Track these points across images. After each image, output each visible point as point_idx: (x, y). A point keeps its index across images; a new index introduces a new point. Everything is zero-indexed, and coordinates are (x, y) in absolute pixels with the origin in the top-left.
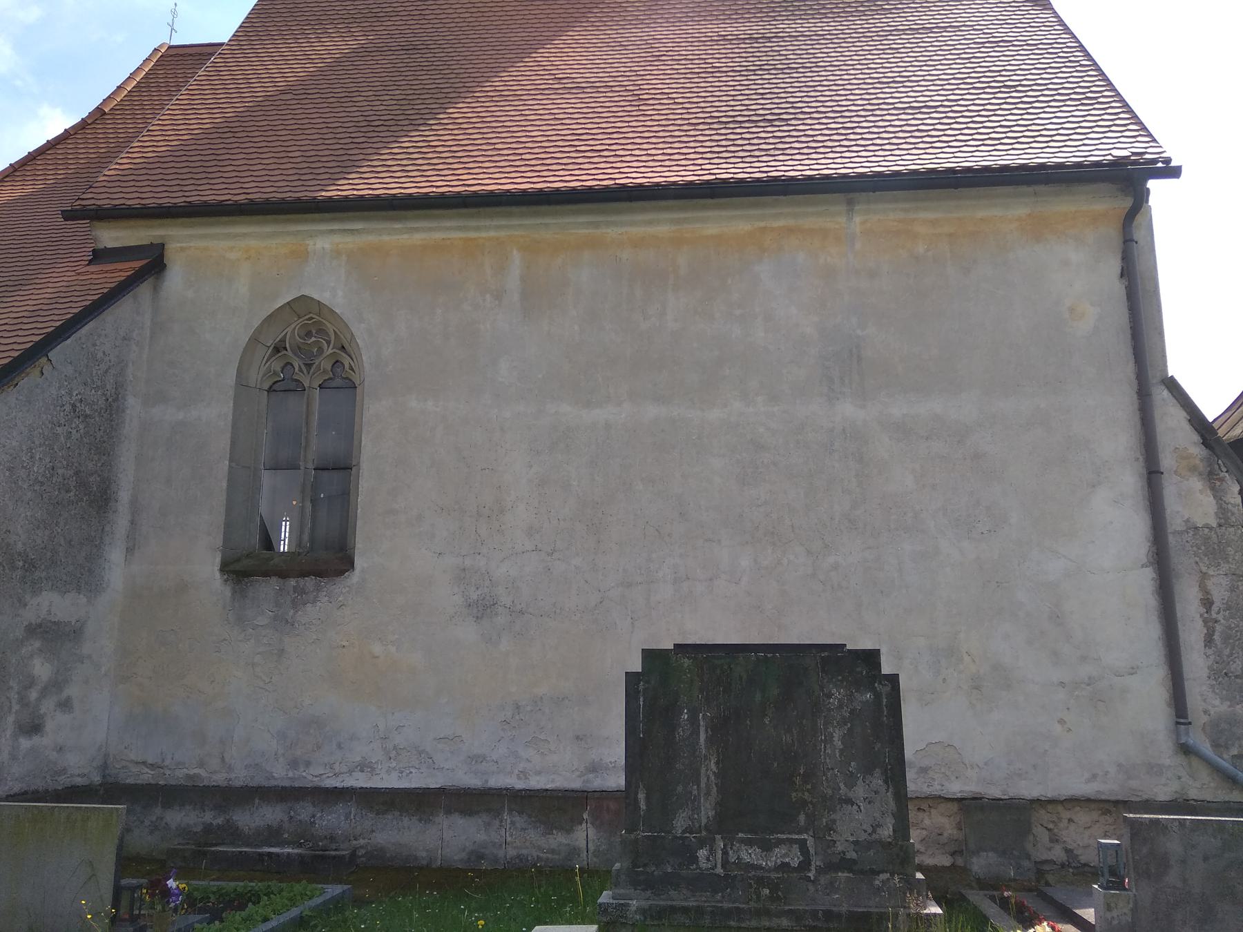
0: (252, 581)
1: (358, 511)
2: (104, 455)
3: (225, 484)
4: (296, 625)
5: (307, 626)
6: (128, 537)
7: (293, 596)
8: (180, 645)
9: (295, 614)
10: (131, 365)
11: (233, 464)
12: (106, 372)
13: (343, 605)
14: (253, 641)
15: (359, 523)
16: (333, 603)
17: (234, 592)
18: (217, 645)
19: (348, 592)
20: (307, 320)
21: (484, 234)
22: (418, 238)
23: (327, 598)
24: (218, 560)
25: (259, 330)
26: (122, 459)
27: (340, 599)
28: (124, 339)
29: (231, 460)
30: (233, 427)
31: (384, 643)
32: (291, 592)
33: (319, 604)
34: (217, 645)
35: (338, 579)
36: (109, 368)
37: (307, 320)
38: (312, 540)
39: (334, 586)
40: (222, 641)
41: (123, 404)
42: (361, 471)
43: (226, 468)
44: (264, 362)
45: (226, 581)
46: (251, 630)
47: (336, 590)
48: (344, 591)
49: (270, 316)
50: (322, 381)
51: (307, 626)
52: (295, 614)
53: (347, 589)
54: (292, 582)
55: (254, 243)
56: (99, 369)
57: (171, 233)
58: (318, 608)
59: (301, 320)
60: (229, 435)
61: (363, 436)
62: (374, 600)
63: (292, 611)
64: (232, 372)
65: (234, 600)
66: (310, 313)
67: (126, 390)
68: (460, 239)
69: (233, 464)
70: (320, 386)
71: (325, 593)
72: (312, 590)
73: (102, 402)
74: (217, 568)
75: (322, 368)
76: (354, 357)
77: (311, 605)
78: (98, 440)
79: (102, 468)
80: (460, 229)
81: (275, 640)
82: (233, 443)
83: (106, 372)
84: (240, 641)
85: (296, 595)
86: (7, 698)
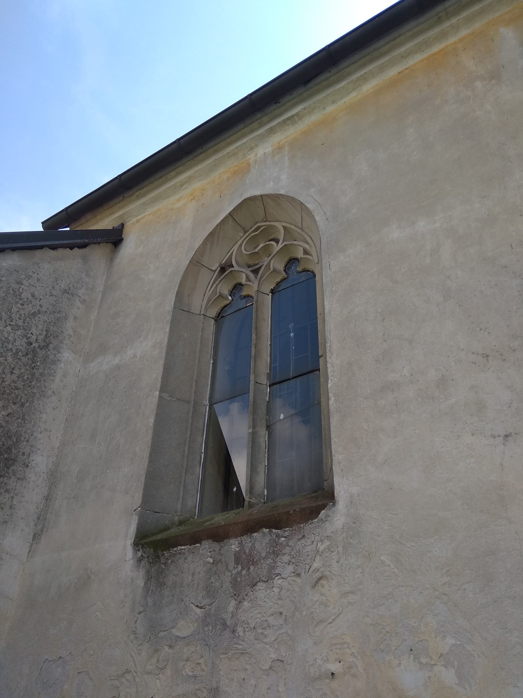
0: (175, 555)
1: (331, 402)
2: (14, 403)
3: (152, 420)
4: (240, 630)
5: (260, 631)
6: (39, 518)
7: (234, 572)
8: (66, 687)
9: (237, 608)
10: (71, 319)
11: (166, 396)
12: (34, 315)
13: (320, 579)
14: (168, 672)
15: (334, 421)
16: (303, 575)
17: (148, 578)
18: (116, 683)
19: (329, 549)
20: (254, 232)
21: (452, 40)
22: (368, 87)
23: (291, 568)
24: (133, 529)
25: (201, 251)
26: (44, 416)
27: (315, 565)
28: (65, 291)
29: (161, 391)
30: (167, 353)
31: (424, 660)
32: (232, 565)
33: (278, 581)
34: (116, 683)
35: (308, 527)
36: (39, 312)
37: (254, 232)
38: (270, 484)
39: (303, 541)
40: (123, 675)
41: (55, 355)
42: (328, 345)
43: (155, 400)
44: (209, 287)
45: (140, 560)
46: (166, 648)
47: (308, 549)
48: (321, 547)
49: (212, 234)
50: (275, 285)
51: (260, 631)
52: (237, 608)
53: (327, 543)
54: (233, 545)
55: (197, 185)
56: (23, 309)
57: (127, 210)
58: (276, 590)
59: (248, 234)
60: (162, 362)
61: (325, 299)
62: (383, 558)
63: (233, 603)
64: (172, 297)
65: (148, 592)
66: (257, 223)
67: (62, 342)
68: (422, 61)
69: (166, 396)
70: (272, 291)
71: (286, 558)
72: (264, 555)
73: (21, 344)
74: (130, 542)
75: (271, 267)
76: (308, 239)
77: (264, 585)
78: (7, 383)
79: (7, 418)
80: (419, 49)
81: (203, 666)
82: (167, 370)
83: (34, 315)
84: (149, 673)
85: (240, 568)
86: (213, 663)
